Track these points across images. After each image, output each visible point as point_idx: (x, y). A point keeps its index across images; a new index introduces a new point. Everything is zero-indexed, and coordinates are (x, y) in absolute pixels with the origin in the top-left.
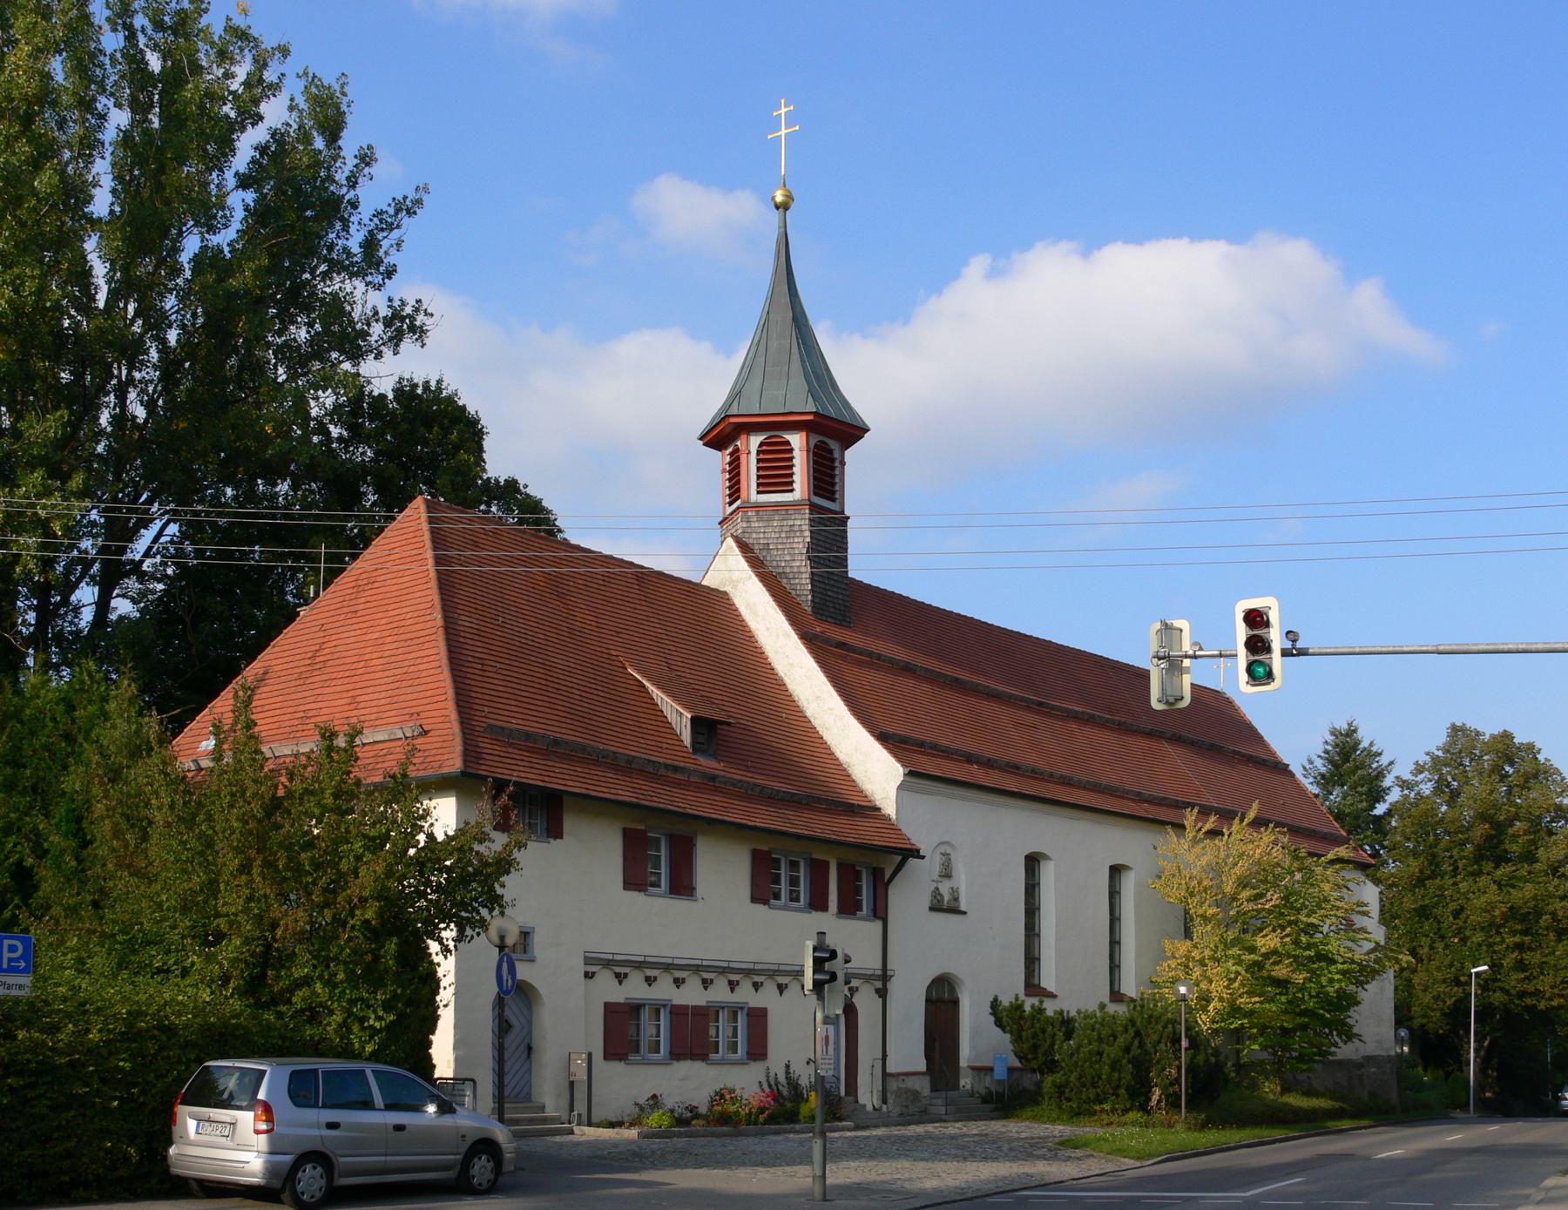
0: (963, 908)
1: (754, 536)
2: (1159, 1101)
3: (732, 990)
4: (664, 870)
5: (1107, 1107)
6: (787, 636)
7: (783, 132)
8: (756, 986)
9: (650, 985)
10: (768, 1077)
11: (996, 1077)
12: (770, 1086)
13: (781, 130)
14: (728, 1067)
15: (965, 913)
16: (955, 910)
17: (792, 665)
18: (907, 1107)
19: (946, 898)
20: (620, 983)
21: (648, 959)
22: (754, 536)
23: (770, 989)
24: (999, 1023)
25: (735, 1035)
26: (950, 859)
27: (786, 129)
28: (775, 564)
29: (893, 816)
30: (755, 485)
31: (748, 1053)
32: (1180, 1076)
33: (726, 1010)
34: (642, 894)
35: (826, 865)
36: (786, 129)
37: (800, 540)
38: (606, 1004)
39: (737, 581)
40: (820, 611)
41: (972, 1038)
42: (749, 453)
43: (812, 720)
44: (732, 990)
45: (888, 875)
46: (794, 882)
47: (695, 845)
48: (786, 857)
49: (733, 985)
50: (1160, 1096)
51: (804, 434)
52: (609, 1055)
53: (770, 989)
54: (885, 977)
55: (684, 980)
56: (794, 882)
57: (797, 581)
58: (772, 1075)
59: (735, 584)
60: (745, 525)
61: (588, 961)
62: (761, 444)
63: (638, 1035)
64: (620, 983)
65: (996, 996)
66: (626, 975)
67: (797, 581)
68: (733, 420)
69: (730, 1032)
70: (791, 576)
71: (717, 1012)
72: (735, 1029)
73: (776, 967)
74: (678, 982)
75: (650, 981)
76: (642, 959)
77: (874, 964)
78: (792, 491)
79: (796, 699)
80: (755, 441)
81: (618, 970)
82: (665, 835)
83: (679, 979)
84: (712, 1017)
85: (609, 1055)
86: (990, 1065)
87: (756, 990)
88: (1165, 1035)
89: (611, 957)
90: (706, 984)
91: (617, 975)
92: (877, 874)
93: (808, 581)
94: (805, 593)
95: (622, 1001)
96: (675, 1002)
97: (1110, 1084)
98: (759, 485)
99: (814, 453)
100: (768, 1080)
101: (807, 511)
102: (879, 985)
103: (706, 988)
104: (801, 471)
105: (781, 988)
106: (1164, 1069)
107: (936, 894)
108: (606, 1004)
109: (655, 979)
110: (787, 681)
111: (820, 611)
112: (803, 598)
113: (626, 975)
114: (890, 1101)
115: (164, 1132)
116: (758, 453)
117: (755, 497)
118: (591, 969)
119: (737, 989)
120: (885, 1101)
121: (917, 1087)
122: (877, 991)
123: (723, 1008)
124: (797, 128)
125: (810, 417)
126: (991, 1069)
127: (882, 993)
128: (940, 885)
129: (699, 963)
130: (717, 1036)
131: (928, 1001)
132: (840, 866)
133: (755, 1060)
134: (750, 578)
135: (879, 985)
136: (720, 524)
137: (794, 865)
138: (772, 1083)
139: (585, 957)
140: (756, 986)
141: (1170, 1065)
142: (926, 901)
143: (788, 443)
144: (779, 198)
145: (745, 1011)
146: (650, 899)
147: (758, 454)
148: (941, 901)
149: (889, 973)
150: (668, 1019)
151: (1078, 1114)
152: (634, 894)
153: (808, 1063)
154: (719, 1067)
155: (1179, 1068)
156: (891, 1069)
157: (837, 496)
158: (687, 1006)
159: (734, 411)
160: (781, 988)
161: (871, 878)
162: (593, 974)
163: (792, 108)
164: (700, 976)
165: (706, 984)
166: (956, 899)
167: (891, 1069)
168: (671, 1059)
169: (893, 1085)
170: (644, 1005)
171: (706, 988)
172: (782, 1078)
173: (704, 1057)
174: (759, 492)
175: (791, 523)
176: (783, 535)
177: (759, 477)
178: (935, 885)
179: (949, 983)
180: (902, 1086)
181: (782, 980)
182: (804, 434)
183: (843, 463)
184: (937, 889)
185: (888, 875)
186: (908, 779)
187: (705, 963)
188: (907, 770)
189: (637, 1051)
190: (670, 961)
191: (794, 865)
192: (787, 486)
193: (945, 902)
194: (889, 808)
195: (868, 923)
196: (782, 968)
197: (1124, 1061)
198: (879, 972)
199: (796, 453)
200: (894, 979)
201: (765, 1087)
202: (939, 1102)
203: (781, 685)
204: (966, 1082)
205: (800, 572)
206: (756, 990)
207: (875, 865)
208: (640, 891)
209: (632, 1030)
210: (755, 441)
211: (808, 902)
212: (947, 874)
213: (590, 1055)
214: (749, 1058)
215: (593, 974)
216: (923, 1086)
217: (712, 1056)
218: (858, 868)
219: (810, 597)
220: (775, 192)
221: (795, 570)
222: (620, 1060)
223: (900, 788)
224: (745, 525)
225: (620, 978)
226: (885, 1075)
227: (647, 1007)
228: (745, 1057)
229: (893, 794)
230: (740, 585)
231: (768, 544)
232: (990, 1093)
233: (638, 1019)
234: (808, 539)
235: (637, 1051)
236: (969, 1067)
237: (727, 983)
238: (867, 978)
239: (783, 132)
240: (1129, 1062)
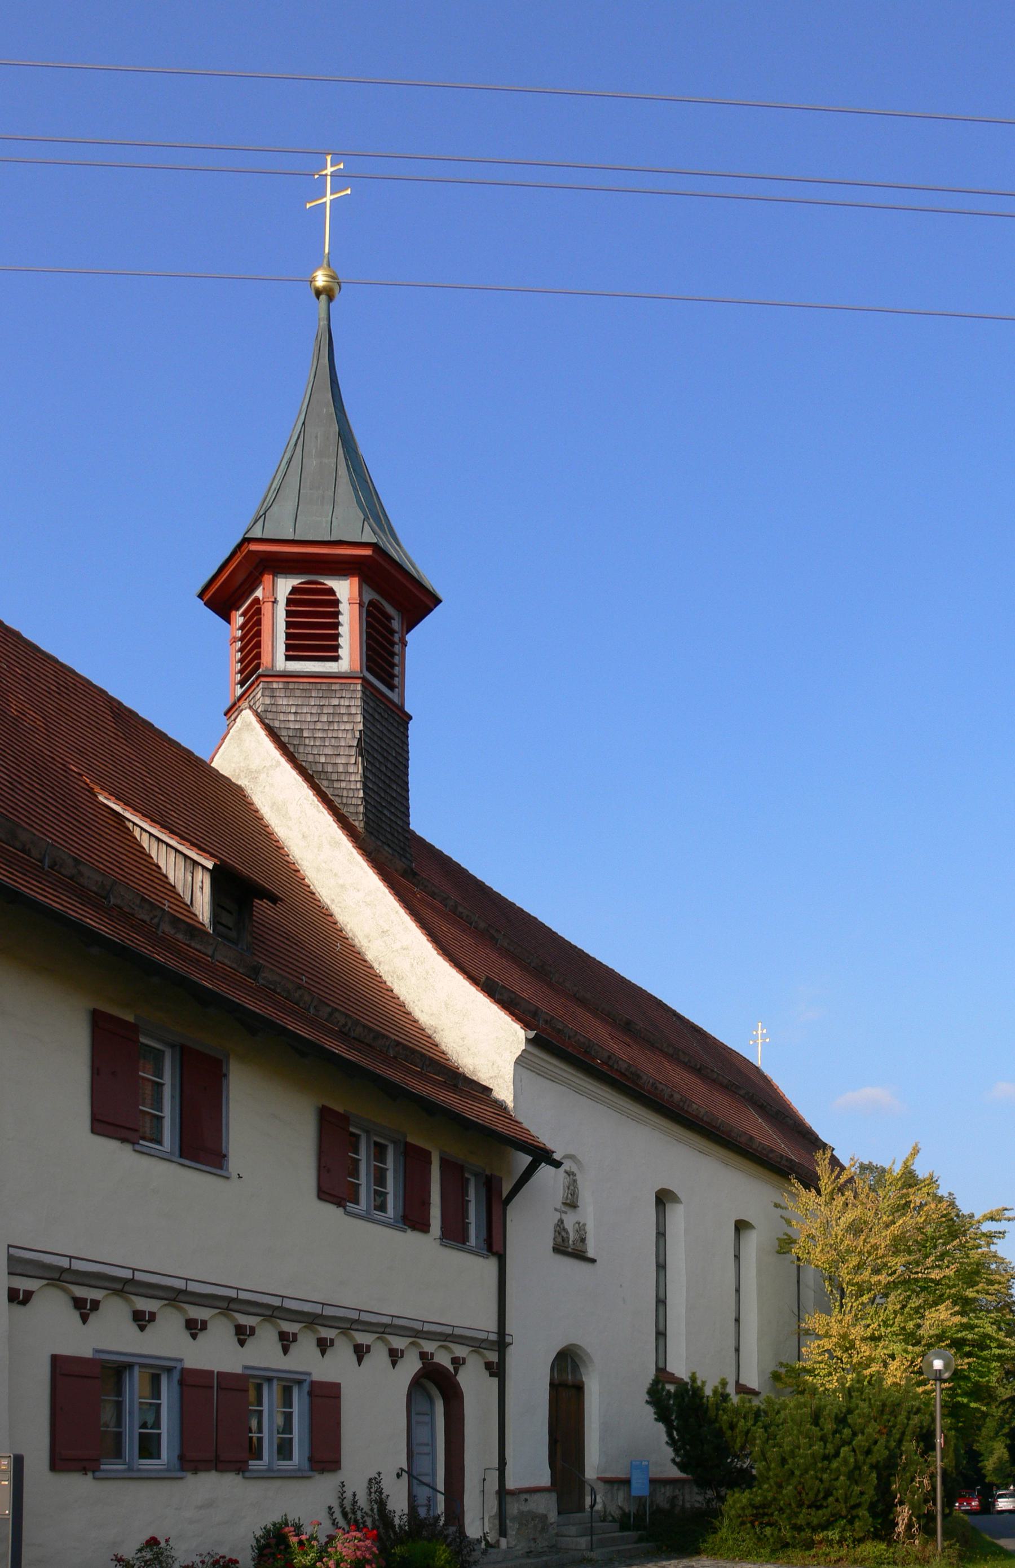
0: (591, 1254)
1: (282, 717)
2: (909, 1526)
3: (286, 1350)
4: (168, 1112)
5: (834, 1535)
6: (337, 844)
7: (329, 198)
8: (324, 1345)
9: (142, 1328)
10: (342, 1499)
11: (634, 1493)
12: (345, 1514)
13: (325, 196)
14: (278, 1483)
15: (593, 1261)
16: (580, 1255)
17: (342, 886)
18: (534, 1540)
19: (572, 1236)
20: (85, 1319)
21: (139, 1276)
22: (282, 717)
23: (343, 1353)
24: (663, 1416)
25: (288, 1427)
26: (575, 1181)
27: (332, 166)
28: (310, 758)
29: (510, 1104)
30: (284, 646)
31: (311, 1459)
32: (934, 1489)
33: (275, 1383)
34: (128, 1148)
35: (426, 1156)
36: (332, 166)
37: (348, 727)
38: (55, 1359)
39: (258, 772)
40: (376, 834)
41: (602, 1439)
42: (275, 602)
43: (376, 966)
44: (286, 1350)
45: (506, 1189)
46: (380, 1178)
47: (225, 1075)
48: (367, 1132)
49: (286, 1341)
50: (910, 1519)
51: (356, 579)
52: (59, 1462)
53: (343, 1353)
54: (501, 1344)
55: (204, 1326)
56: (380, 1178)
57: (343, 785)
58: (348, 1495)
59: (254, 775)
60: (268, 701)
61: (17, 1266)
62: (294, 590)
63: (119, 1422)
64: (85, 1319)
65: (694, 1374)
66: (95, 1305)
67: (343, 785)
68: (254, 547)
69: (280, 1421)
70: (334, 777)
71: (259, 1388)
72: (288, 1417)
73: (354, 1315)
74: (194, 1328)
75: (142, 1320)
76: (127, 1274)
77: (486, 1323)
78: (336, 659)
79: (350, 935)
80: (285, 586)
81: (80, 1292)
82: (172, 1046)
83: (195, 1321)
84: (252, 1394)
85: (59, 1462)
86: (622, 1475)
87: (323, 1353)
88: (909, 1431)
89: (64, 1263)
90: (243, 1335)
91: (79, 1303)
92: (490, 1186)
93: (359, 785)
94: (354, 801)
95: (88, 1354)
96: (189, 1364)
97: (846, 1502)
98: (288, 647)
99: (368, 612)
100: (342, 1506)
101: (359, 687)
102: (493, 1357)
103: (242, 1343)
104: (351, 632)
105: (360, 1352)
106: (913, 1480)
107: (560, 1228)
108: (55, 1359)
109: (153, 1317)
110: (335, 909)
111: (376, 834)
112: (352, 809)
113: (95, 1305)
114: (511, 1532)
115: (100, 1467)
116: (289, 602)
117: (282, 664)
118: (24, 1284)
119: (294, 1348)
120: (503, 1532)
121: (541, 1510)
122: (488, 1366)
123: (269, 1380)
124: (349, 192)
125: (368, 552)
126: (626, 1482)
127: (497, 1370)
128: (564, 1216)
129: (232, 1294)
130: (260, 1430)
131: (552, 1385)
132: (444, 1163)
133: (322, 1471)
134: (278, 764)
135: (493, 1357)
136: (226, 714)
137: (380, 1153)
138: (348, 1509)
139: (11, 1258)
140: (324, 1345)
141: (922, 1473)
142: (548, 1241)
143: (331, 592)
144: (321, 279)
145: (306, 1387)
146: (145, 1162)
147: (288, 605)
148: (565, 1240)
149: (508, 1339)
150: (176, 1395)
151: (786, 1545)
152: (111, 1146)
153: (399, 1476)
154: (263, 1485)
155: (932, 1476)
156: (510, 1485)
157: (396, 681)
158: (212, 1372)
159: (257, 533)
160: (360, 1352)
161: (483, 1191)
162: (28, 1295)
163: (341, 166)
164: (234, 1319)
165: (243, 1335)
166: (583, 1240)
167: (510, 1485)
168: (182, 1469)
169: (514, 1508)
170: (130, 1366)
171: (242, 1343)
172: (363, 1501)
173: (239, 1467)
174: (288, 658)
175: (335, 702)
176: (324, 718)
177: (288, 636)
178: (557, 1215)
179: (573, 1361)
180: (525, 1508)
181: (363, 1338)
182: (356, 579)
183: (404, 644)
184: (561, 1221)
185: (506, 1189)
186: (531, 1049)
187: (243, 1296)
188: (532, 1034)
189: (118, 1453)
190: (180, 1284)
191: (380, 1153)
192: (330, 651)
193: (571, 1242)
194: (504, 1092)
195: (481, 1259)
196: (365, 1317)
197: (865, 1468)
198: (493, 1337)
199: (344, 607)
200: (511, 1347)
201: (338, 1515)
202: (573, 1530)
203: (327, 915)
204: (600, 1501)
205: (347, 773)
206: (323, 1353)
207: (488, 1172)
208: (124, 1140)
209: (107, 1415)
210: (285, 586)
211: (401, 1212)
212: (571, 1204)
213: (18, 1462)
214: (312, 1469)
215: (28, 1295)
216: (546, 1506)
217: (253, 1464)
218: (467, 1175)
219: (361, 809)
220: (315, 271)
221: (341, 769)
222: (85, 1470)
223: (521, 1062)
224: (268, 701)
225: (85, 1309)
226: (503, 1493)
227: (136, 1370)
228: (306, 1465)
229: (508, 1070)
230: (263, 776)
231: (302, 730)
232: (625, 1515)
233: (119, 1391)
234: (361, 727)
235: (118, 1453)
236: (599, 1479)
237: (276, 1337)
238: (477, 1345)
239: (329, 198)
240: (873, 1467)
